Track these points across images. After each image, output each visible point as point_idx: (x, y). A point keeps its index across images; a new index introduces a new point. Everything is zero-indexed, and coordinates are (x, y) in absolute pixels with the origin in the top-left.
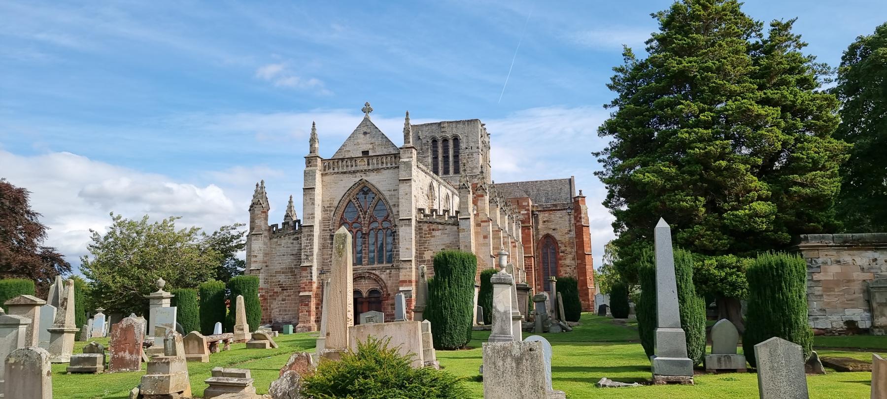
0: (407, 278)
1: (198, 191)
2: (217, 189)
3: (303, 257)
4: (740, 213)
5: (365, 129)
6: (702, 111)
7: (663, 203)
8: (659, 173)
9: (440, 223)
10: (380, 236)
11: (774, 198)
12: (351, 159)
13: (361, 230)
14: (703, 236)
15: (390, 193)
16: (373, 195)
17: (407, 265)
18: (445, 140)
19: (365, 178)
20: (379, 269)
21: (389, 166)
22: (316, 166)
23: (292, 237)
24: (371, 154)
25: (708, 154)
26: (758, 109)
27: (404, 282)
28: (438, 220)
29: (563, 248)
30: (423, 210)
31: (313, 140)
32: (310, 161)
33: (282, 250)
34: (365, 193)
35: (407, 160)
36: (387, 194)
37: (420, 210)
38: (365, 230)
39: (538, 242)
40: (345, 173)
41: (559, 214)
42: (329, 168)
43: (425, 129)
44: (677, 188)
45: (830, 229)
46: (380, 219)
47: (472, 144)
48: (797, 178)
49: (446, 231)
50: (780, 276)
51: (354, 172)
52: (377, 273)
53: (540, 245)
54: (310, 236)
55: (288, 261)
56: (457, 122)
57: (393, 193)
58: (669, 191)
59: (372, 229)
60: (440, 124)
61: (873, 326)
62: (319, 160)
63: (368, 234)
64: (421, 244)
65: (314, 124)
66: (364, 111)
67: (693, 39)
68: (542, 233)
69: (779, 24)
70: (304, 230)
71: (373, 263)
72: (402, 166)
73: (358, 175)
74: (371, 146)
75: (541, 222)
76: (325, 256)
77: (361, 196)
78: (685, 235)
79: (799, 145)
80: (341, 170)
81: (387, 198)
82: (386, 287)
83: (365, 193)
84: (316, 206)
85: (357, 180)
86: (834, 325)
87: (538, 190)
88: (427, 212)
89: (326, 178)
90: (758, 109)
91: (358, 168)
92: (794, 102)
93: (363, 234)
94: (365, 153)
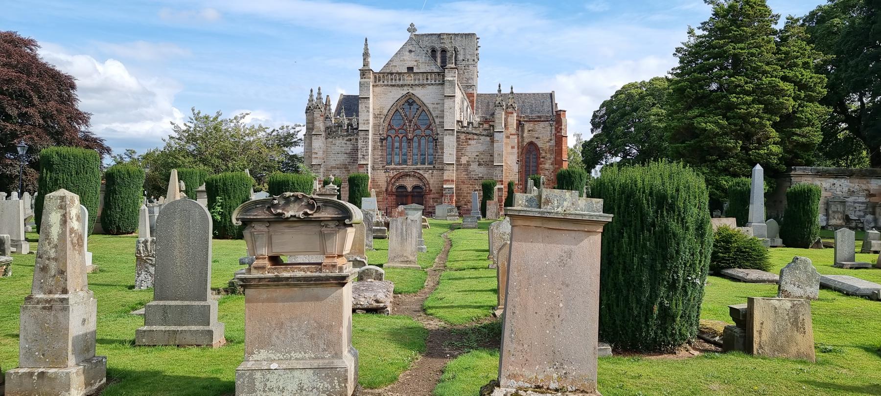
0: (450, 178)
1: (100, 68)
2: (118, 64)
3: (360, 156)
4: (762, 152)
5: (410, 48)
6: (746, 83)
7: (714, 143)
8: (716, 123)
10: (423, 141)
11: (781, 143)
12: (400, 74)
13: (406, 136)
14: (735, 166)
17: (450, 167)
18: (444, 51)
19: (411, 91)
20: (423, 169)
21: (433, 82)
23: (346, 138)
25: (749, 114)
26: (782, 85)
27: (448, 181)
29: (544, 155)
30: (461, 122)
31: (366, 55)
32: (364, 73)
33: (337, 149)
34: (410, 104)
36: (431, 107)
37: (458, 122)
38: (410, 136)
40: (394, 86)
41: (542, 124)
43: (426, 39)
44: (726, 134)
45: (809, 163)
46: (423, 128)
47: (468, 57)
48: (798, 131)
50: (809, 197)
51: (402, 86)
52: (421, 172)
53: (524, 151)
54: (366, 139)
55: (342, 159)
56: (455, 35)
57: (436, 106)
58: (721, 135)
60: (440, 35)
61: (828, 225)
64: (460, 150)
66: (409, 30)
67: (743, 31)
68: (527, 141)
69: (792, 19)
70: (360, 133)
71: (417, 164)
72: (447, 84)
73: (405, 88)
74: (415, 63)
75: (526, 131)
76: (376, 157)
77: (406, 106)
78: (724, 164)
79: (800, 109)
80: (390, 83)
82: (428, 184)
83: (410, 104)
87: (523, 102)
89: (377, 89)
90: (782, 85)
91: (406, 82)
92: (801, 80)
93: (408, 139)
94: (410, 69)
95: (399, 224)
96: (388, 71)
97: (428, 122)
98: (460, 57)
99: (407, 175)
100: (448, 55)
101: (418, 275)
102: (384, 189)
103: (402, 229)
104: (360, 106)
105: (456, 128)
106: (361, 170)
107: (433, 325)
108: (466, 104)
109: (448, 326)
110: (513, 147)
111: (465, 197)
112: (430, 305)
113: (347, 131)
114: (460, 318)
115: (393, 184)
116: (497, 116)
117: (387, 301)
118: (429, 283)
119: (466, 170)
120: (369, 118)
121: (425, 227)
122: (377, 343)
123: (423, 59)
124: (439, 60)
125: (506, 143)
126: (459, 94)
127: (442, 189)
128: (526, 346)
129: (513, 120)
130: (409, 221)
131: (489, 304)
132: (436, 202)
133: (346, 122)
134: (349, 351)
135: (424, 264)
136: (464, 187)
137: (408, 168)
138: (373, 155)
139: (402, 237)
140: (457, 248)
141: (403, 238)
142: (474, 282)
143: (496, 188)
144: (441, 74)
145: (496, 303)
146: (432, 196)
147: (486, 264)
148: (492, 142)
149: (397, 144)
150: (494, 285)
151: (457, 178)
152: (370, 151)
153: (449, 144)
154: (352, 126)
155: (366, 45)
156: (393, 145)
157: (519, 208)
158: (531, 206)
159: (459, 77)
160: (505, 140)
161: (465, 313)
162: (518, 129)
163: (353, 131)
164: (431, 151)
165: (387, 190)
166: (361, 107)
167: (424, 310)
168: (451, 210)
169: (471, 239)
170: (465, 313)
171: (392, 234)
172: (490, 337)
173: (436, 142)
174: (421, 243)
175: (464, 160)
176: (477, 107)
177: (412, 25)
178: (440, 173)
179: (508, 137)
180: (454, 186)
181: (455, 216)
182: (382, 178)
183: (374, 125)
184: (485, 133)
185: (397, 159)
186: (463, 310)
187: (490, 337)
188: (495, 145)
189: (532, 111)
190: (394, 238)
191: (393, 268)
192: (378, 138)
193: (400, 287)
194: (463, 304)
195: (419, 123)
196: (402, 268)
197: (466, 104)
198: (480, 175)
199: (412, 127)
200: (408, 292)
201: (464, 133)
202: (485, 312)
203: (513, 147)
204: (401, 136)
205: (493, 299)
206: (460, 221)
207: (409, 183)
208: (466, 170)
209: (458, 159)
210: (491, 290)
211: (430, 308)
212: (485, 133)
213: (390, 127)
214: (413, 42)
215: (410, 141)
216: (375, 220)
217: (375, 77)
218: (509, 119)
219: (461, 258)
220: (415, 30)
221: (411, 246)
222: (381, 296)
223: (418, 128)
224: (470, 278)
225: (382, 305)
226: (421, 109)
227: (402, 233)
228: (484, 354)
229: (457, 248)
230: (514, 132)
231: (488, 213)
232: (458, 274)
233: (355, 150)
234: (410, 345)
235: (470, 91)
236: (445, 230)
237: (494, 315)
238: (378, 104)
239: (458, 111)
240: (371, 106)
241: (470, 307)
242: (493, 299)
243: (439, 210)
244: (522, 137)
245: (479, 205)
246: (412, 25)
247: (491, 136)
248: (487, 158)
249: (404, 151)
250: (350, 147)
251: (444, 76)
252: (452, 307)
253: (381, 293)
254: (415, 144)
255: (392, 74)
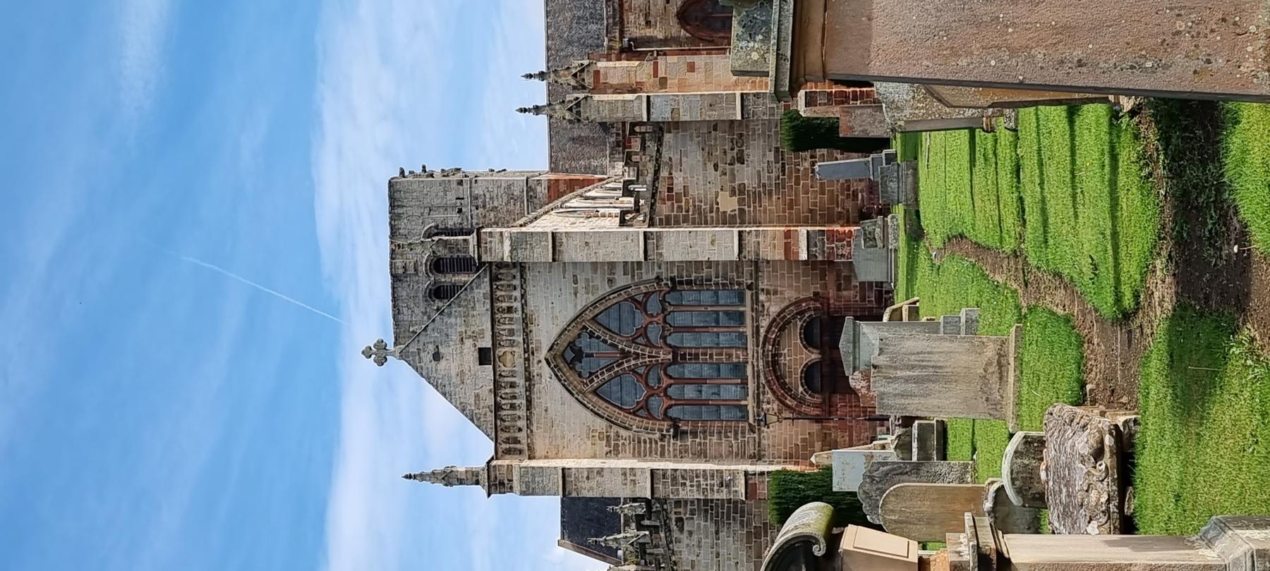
0: (780, 242)
3: (724, 495)
5: (427, 357)
9: (657, 172)
10: (680, 319)
12: (497, 386)
13: (665, 366)
15: (581, 291)
16: (585, 336)
17: (750, 241)
18: (437, 265)
19: (543, 354)
20: (756, 320)
21: (517, 293)
22: (510, 467)
23: (676, 534)
24: (487, 343)
27: (787, 249)
28: (649, 178)
30: (624, 213)
31: (448, 478)
32: (496, 483)
34: (579, 355)
35: (507, 243)
36: (584, 300)
37: (623, 223)
38: (664, 356)
39: (696, 39)
42: (516, 441)
43: (406, 316)
46: (641, 320)
47: (451, 197)
49: (676, 158)
51: (529, 378)
52: (765, 323)
56: (392, 206)
57: (581, 284)
59: (664, 338)
60: (396, 278)
62: (494, 463)
63: (674, 350)
64: (700, 216)
65: (409, 477)
66: (381, 361)
68: (675, 29)
70: (660, 493)
71: (742, 336)
72: (521, 256)
73: (535, 369)
74: (468, 343)
75: (649, 32)
76: (724, 449)
77: (583, 366)
80: (522, 412)
81: (592, 298)
82: (798, 303)
83: (579, 355)
84: (606, 466)
85: (546, 371)
86: (1217, 406)
87: (570, 43)
88: (629, 202)
89: (540, 447)
91: (520, 369)
93: (675, 361)
94: (484, 356)
95: (890, 388)
96: (491, 417)
97: (626, 307)
98: (453, 220)
99: (774, 364)
100: (443, 252)
101: (1036, 333)
102: (815, 427)
103: (907, 380)
104: (586, 494)
105: (640, 229)
106: (764, 490)
107: (1163, 292)
108: (575, 203)
109: (1167, 247)
110: (691, 68)
111: (833, 199)
112: (1111, 300)
113: (654, 529)
114: (1143, 213)
115: (801, 401)
116: (606, 116)
117: (1101, 422)
118: (1057, 301)
119: (757, 196)
120: (623, 471)
121: (914, 312)
122: (1210, 457)
123: (455, 324)
124: (463, 278)
125: (682, 85)
126: (549, 223)
127: (811, 263)
128: (1180, 25)
129: (616, 69)
130: (882, 360)
131: (1105, 127)
132: (848, 279)
133: (632, 532)
134: (1210, 544)
135: (1010, 317)
136: (805, 201)
137: (754, 359)
138: (719, 457)
139: (928, 380)
140: (968, 219)
141: (932, 376)
142: (1050, 171)
143: (803, 111)
144: (496, 271)
145: (1101, 109)
146: (832, 293)
147: (1005, 137)
148: (676, 125)
149: (690, 392)
150: (1059, 112)
151: (780, 221)
152: (709, 466)
153: (685, 245)
154: (639, 518)
155: (422, 477)
156: (691, 403)
157: (772, 59)
158: (767, 23)
159: (506, 224)
160: (671, 91)
161: (1131, 199)
162: (640, 56)
163: (656, 513)
164: (706, 297)
165: (817, 420)
166: (589, 490)
167: (1126, 317)
168: (870, 239)
169: (946, 180)
170: (1131, 199)
171: (934, 405)
172: (1190, 128)
173: (682, 281)
174: (952, 325)
175: (729, 204)
176: (587, 169)
177: (367, 353)
178: (765, 269)
179: (663, 83)
180: (803, 231)
181: (885, 225)
182: (782, 432)
183: (638, 454)
184: (652, 147)
185: (730, 392)
186: (1123, 203)
187: (1190, 128)
188: (685, 117)
189: (595, 17)
190: (933, 401)
191: (1018, 404)
192: (673, 444)
193: (1066, 386)
194: (1105, 204)
195: (629, 331)
196: (1018, 380)
197: (575, 203)
198: (771, 156)
199: (638, 348)
200: (1081, 362)
201: (655, 204)
202: (1126, 138)
203: (691, 68)
204: (666, 381)
205: (1094, 114)
206: (899, 211)
207: (797, 356)
208: (757, 196)
209: (727, 220)
210: (1071, 122)
211: (1118, 300)
212: (652, 147)
213: (642, 410)
214: (413, 349)
215: (679, 356)
216: (892, 455)
217: (508, 452)
218: (614, 81)
219: (991, 207)
220: (381, 345)
221: (955, 354)
222: (1083, 443)
223: (644, 332)
224: (1041, 184)
225: (1108, 441)
226: (592, 327)
227: (917, 380)
228: (1235, 142)
229: (968, 219)
230: (648, 66)
231: (877, 132)
232: (1033, 218)
233: (706, 507)
234: (1216, 359)
235: (542, 191)
236: (922, 252)
237: (1133, 113)
238: (579, 444)
239: (594, 222)
240: (586, 463)
241: (1113, 183)
242: (1094, 114)
243: (869, 270)
244: (665, 42)
245: (856, 159)
246: (367, 353)
247: (660, 130)
248: (722, 141)
249: (706, 371)
250: (700, 524)
251: (501, 265)
252: (1115, 235)
253: (1077, 438)
254: (688, 341)
255: (498, 407)
